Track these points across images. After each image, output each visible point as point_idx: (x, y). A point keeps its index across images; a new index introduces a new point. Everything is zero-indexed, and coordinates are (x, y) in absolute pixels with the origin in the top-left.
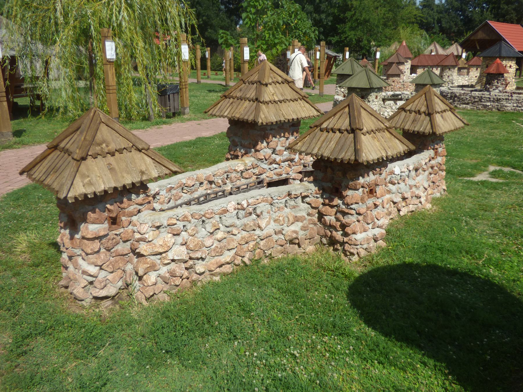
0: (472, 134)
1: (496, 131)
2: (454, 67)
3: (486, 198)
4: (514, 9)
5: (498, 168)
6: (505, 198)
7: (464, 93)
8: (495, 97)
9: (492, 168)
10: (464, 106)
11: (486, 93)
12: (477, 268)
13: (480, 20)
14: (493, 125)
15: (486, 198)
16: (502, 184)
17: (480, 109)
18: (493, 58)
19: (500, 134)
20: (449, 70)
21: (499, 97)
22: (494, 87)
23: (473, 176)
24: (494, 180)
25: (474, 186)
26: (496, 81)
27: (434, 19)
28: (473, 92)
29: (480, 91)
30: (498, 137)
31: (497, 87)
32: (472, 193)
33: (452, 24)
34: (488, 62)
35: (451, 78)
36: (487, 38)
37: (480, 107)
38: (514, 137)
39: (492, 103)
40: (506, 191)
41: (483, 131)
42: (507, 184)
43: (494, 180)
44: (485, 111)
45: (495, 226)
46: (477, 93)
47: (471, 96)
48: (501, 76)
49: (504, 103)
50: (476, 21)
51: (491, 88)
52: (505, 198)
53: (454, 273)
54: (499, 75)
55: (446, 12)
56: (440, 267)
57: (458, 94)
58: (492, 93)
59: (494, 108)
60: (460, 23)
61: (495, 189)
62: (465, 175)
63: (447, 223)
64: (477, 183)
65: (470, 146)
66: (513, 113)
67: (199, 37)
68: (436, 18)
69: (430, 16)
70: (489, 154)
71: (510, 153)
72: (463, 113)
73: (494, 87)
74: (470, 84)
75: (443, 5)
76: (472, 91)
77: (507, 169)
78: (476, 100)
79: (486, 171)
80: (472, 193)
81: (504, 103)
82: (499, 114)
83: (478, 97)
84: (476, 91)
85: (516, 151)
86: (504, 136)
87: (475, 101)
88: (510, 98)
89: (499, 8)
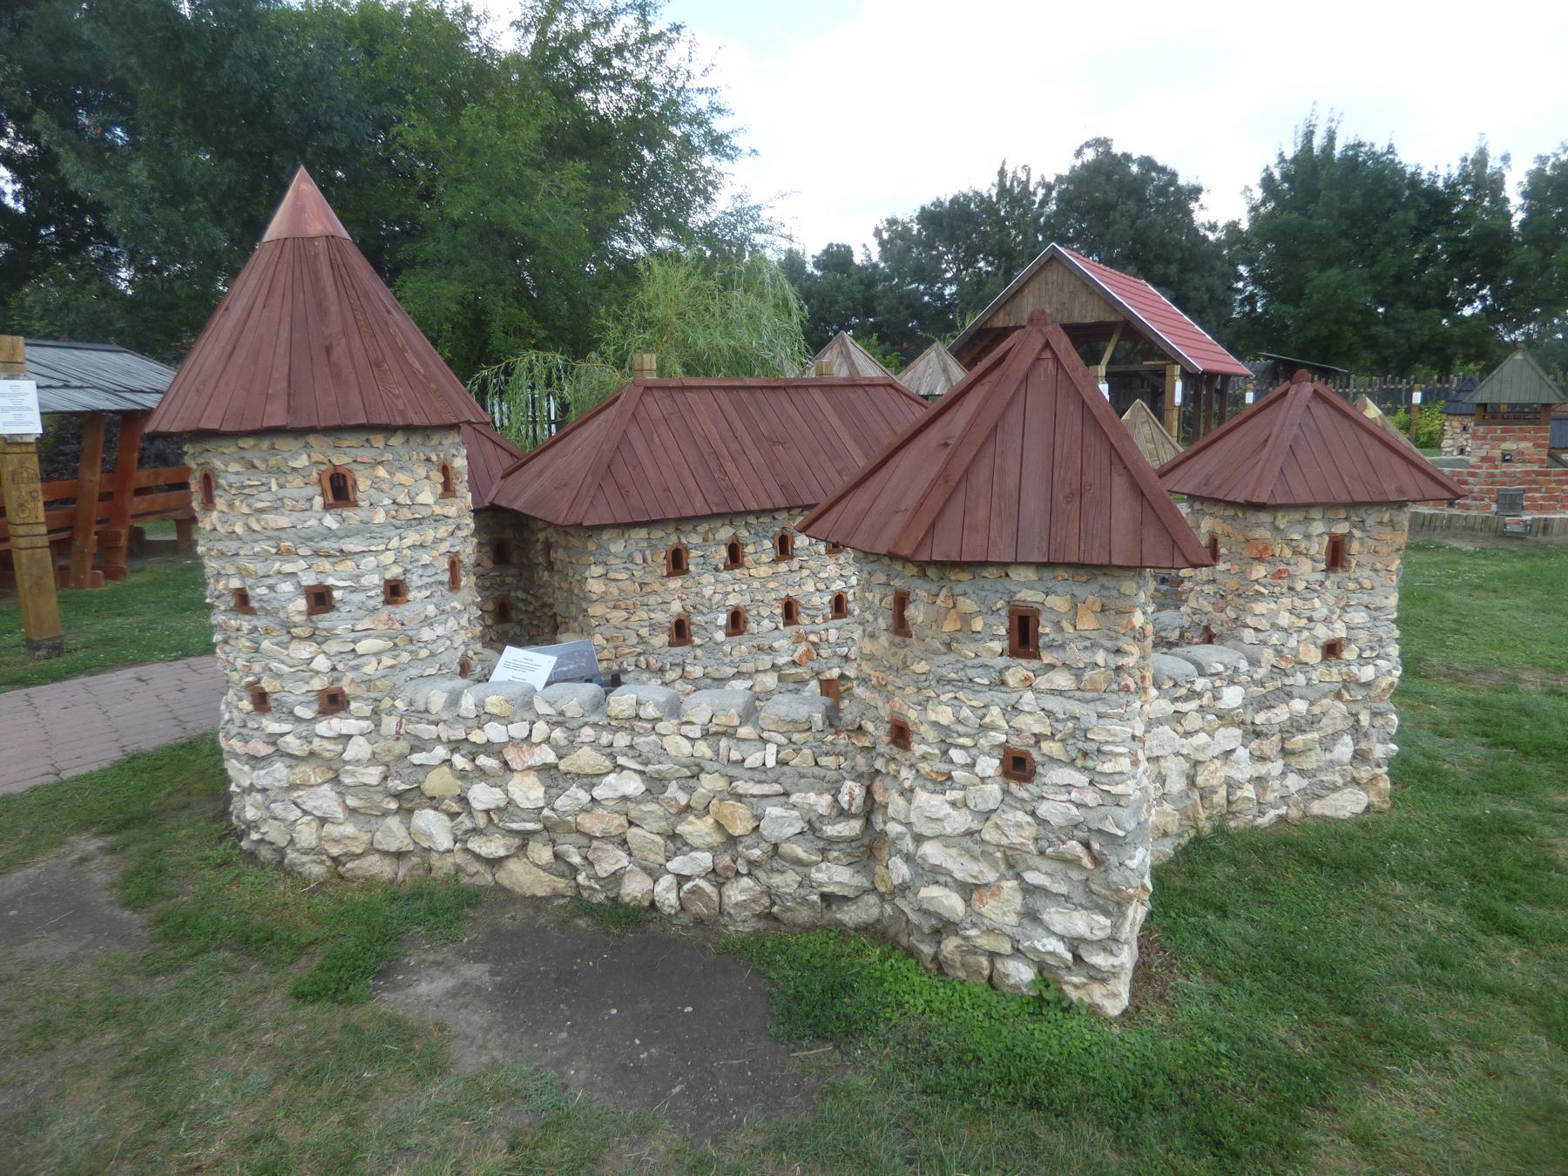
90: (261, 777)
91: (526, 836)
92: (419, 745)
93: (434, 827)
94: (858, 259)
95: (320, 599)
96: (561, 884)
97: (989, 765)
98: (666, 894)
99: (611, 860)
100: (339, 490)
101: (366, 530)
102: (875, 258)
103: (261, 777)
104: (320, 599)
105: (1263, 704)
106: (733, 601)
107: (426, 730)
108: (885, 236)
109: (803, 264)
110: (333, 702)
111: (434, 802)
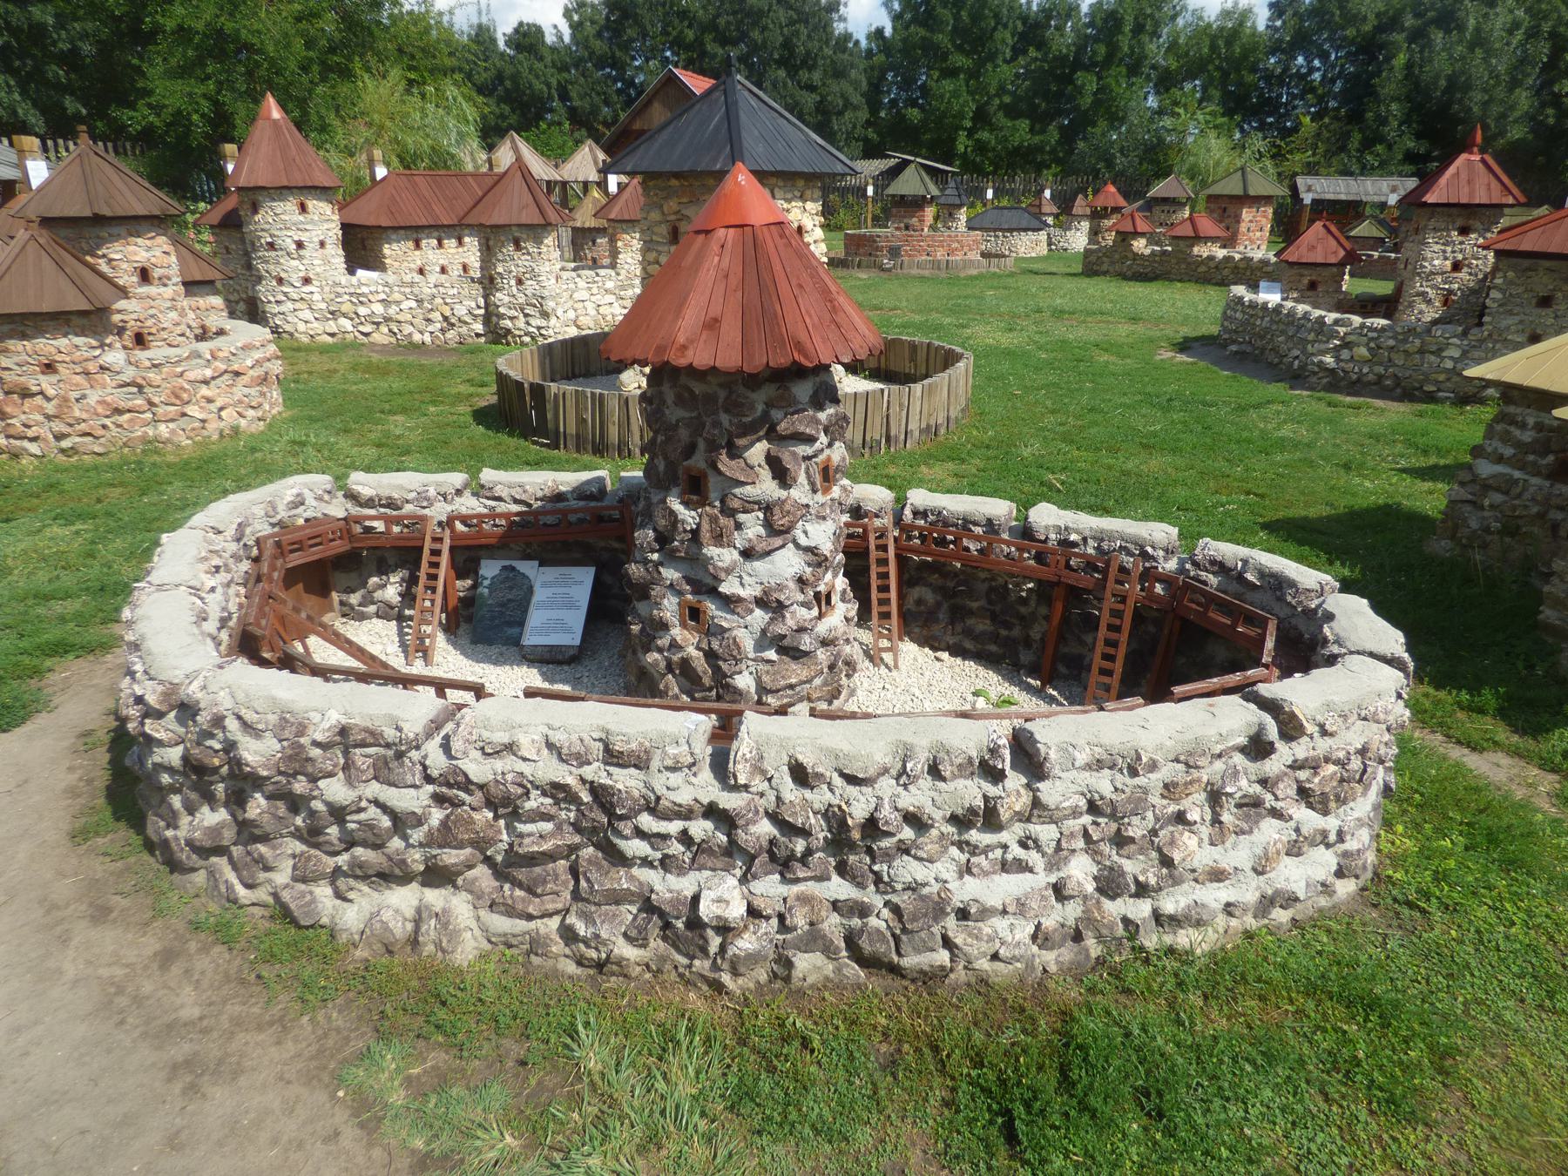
2: (537, 231)
8: (806, 804)
20: (518, 247)
21: (859, 807)
22: (753, 527)
26: (757, 452)
27: (548, 85)
31: (778, 529)
33: (596, 99)
34: (672, 204)
35: (530, 285)
39: (770, 887)
48: (803, 390)
49: (933, 870)
51: (719, 539)
55: (577, 66)
57: (257, 753)
59: (814, 940)
60: (615, 98)
68: (554, 83)
69: (537, 77)
73: (753, 527)
75: (568, 48)
83: (558, 791)
90: (282, 308)
91: (378, 324)
92: (338, 295)
93: (346, 324)
94: (550, 39)
95: (300, 245)
96: (393, 340)
97: (513, 282)
98: (427, 338)
99: (408, 329)
100: (303, 208)
101: (312, 222)
102: (567, 39)
103: (282, 308)
104: (300, 245)
105: (623, 288)
106: (442, 262)
107: (339, 290)
108: (576, 18)
109: (494, 41)
110: (307, 281)
111: (345, 315)
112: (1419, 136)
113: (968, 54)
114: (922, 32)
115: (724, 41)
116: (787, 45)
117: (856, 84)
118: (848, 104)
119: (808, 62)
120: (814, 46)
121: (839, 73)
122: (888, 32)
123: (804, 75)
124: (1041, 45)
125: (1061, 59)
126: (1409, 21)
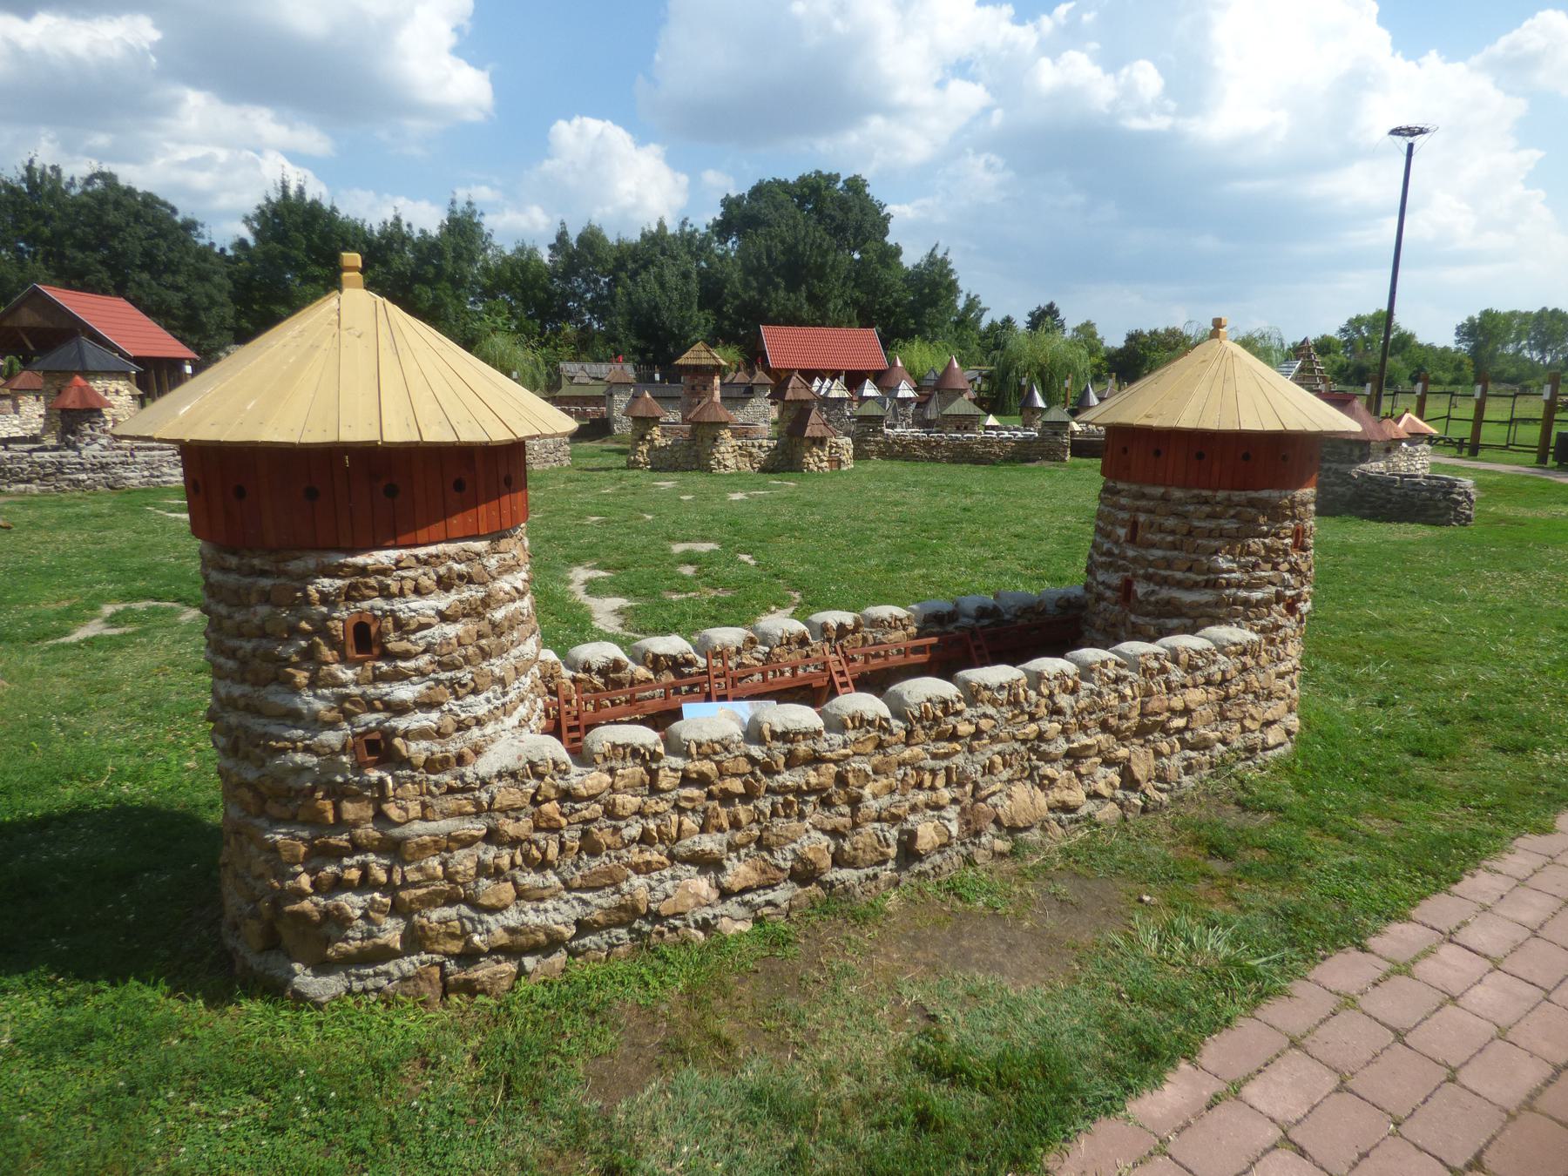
0: (51, 547)
1: (109, 534)
3: (101, 669)
4: (102, 263)
5: (121, 607)
6: (144, 659)
7: (12, 458)
9: (108, 610)
10: (22, 486)
11: (70, 453)
12: (96, 795)
13: (20, 280)
14: (100, 521)
15: (101, 669)
16: (133, 634)
17: (64, 491)
18: (68, 374)
19: (120, 537)
22: (88, 440)
23: (66, 633)
24: (116, 631)
25: (71, 653)
28: (35, 454)
29: (55, 449)
30: (116, 545)
31: (94, 440)
32: (69, 668)
36: (48, 324)
37: (63, 484)
38: (150, 539)
40: (143, 645)
41: (79, 537)
42: (144, 633)
43: (116, 631)
44: (78, 494)
45: (131, 714)
46: (46, 455)
47: (32, 464)
49: (120, 471)
50: (10, 282)
52: (144, 659)
53: (47, 821)
54: (91, 412)
56: (12, 823)
58: (84, 453)
61: (120, 647)
62: (46, 636)
63: (14, 738)
64: (77, 646)
65: (48, 573)
66: (145, 491)
67: (395, 777)
70: (99, 582)
71: (143, 572)
72: (22, 503)
73: (88, 440)
74: (29, 434)
76: (30, 451)
77: (141, 606)
78: (49, 471)
79: (97, 617)
80: (69, 668)
81: (120, 471)
82: (114, 496)
84: (44, 449)
85: (155, 567)
86: (128, 540)
87: (43, 474)
88: (130, 460)
89: (62, 256)
112: (639, 337)
113: (322, 266)
114: (280, 247)
115: (83, 246)
116: (147, 253)
117: (220, 288)
118: (213, 303)
119: (171, 267)
120: (175, 256)
121: (203, 277)
122: (251, 241)
123: (168, 278)
124: (385, 263)
125: (401, 275)
126: (630, 266)
